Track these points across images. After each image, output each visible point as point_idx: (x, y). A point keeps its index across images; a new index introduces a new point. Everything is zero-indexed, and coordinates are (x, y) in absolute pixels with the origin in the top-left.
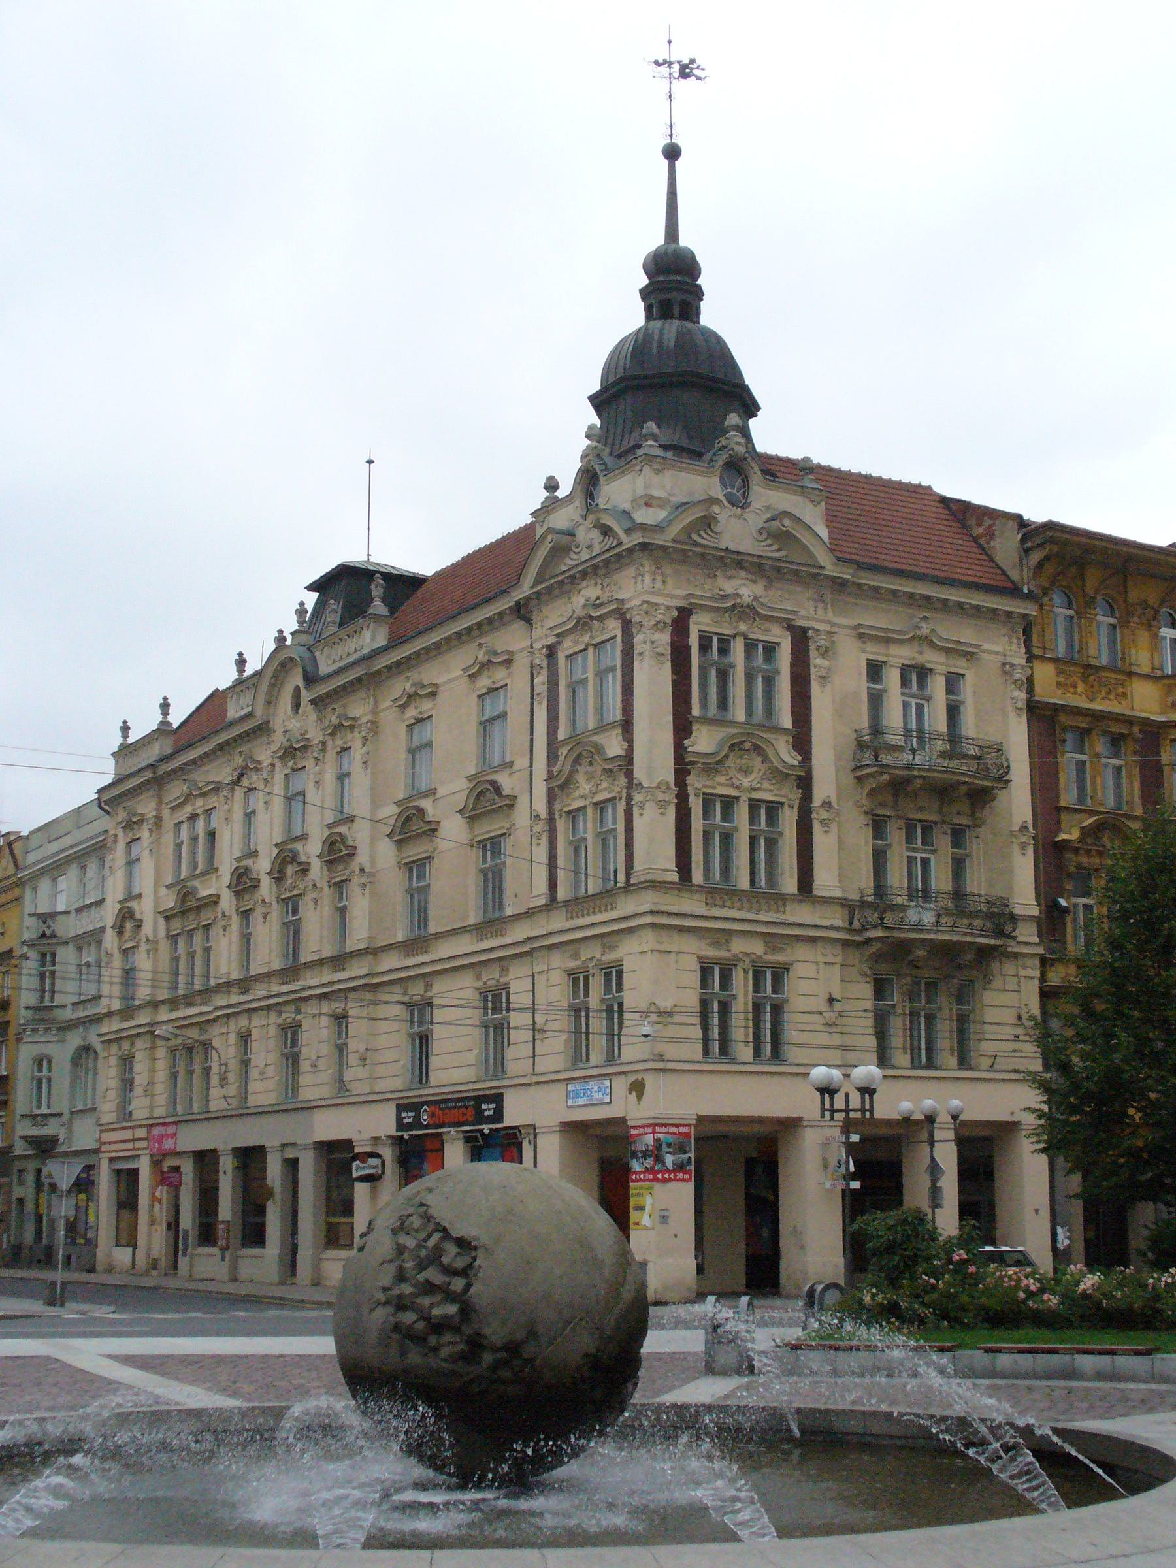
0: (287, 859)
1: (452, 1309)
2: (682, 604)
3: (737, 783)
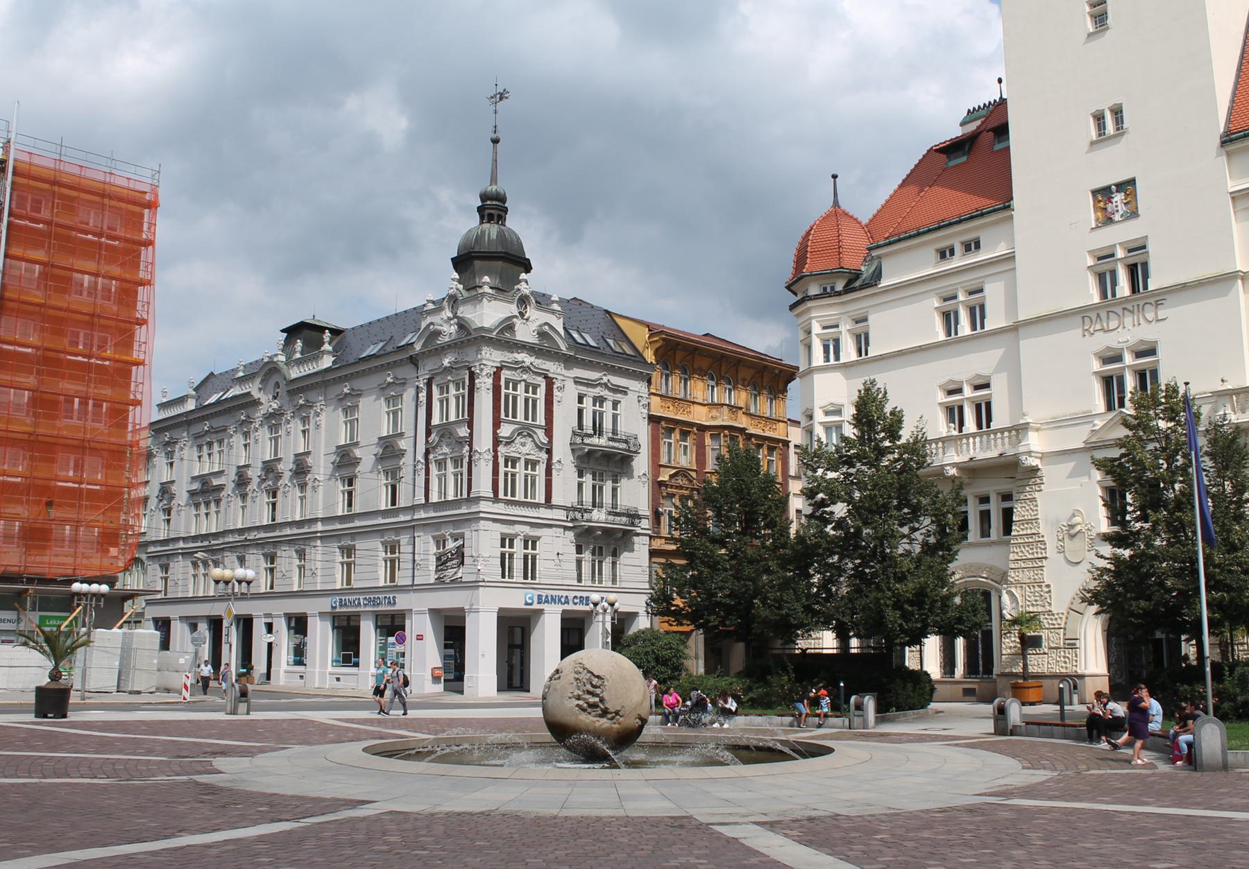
0: (270, 468)
1: (597, 699)
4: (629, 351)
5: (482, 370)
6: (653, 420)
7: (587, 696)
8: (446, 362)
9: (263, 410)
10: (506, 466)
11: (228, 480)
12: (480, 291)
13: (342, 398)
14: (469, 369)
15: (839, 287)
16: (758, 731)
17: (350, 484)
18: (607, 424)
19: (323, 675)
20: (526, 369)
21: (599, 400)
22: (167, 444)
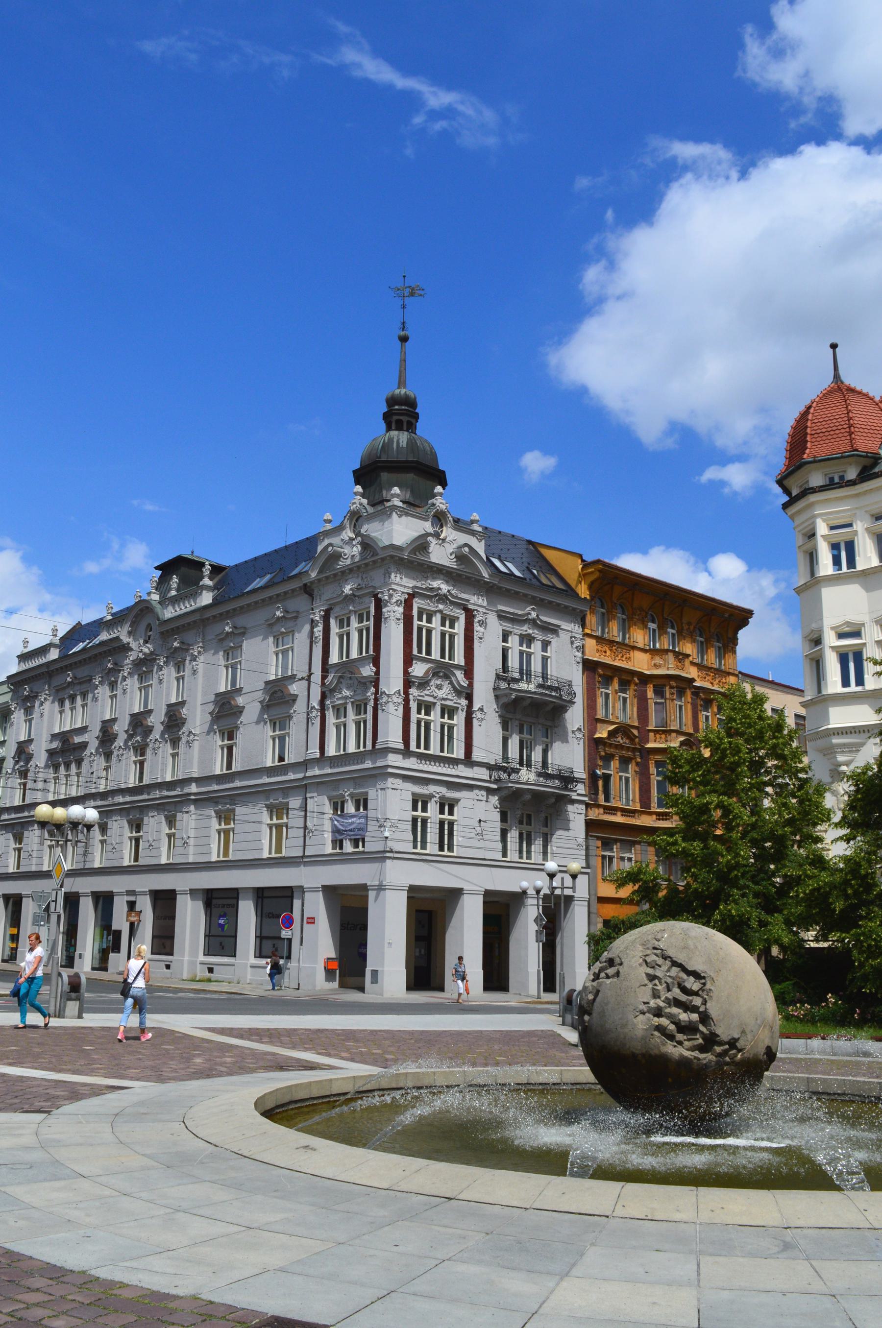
0: (138, 722)
1: (695, 1017)
2: (410, 591)
3: (436, 695)
4: (559, 585)
5: (391, 596)
6: (589, 666)
7: (675, 1010)
8: (347, 589)
9: (133, 656)
10: (419, 712)
11: (92, 738)
12: (388, 504)
13: (223, 638)
14: (375, 596)
15: (852, 474)
16: (841, 1066)
17: (230, 738)
18: (536, 666)
19: (192, 964)
20: (443, 598)
21: (527, 639)
22: (27, 699)
